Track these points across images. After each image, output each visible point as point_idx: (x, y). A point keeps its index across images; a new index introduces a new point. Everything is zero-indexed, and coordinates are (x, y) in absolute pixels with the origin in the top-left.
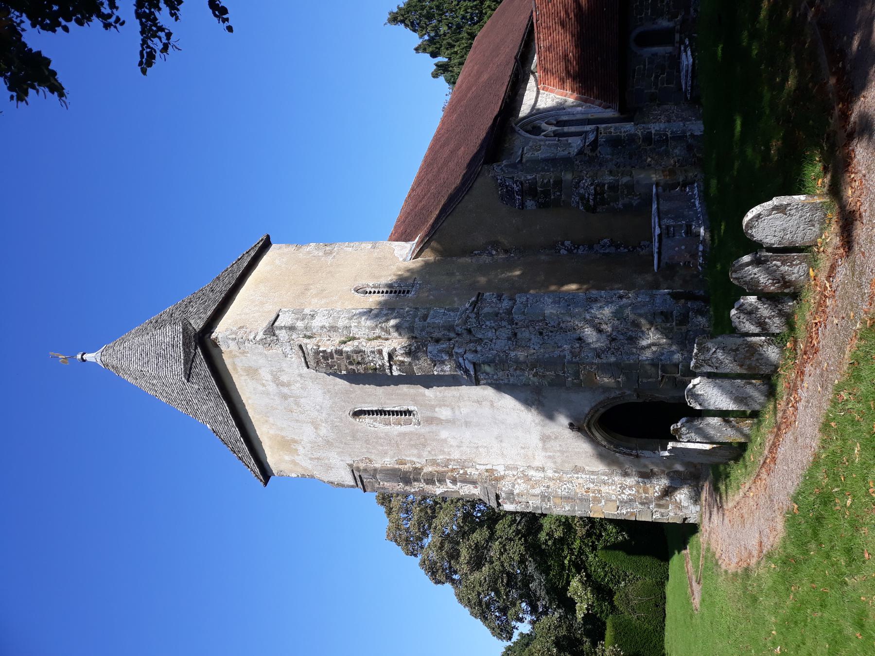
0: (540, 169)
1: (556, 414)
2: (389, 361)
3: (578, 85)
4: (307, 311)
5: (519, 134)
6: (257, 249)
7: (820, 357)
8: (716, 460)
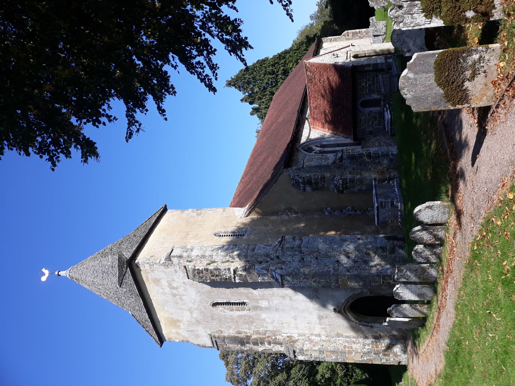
0: (313, 171)
2: (234, 274)
3: (331, 126)
4: (189, 247)
5: (301, 152)
6: (160, 212)
7: (453, 275)
8: (412, 327)
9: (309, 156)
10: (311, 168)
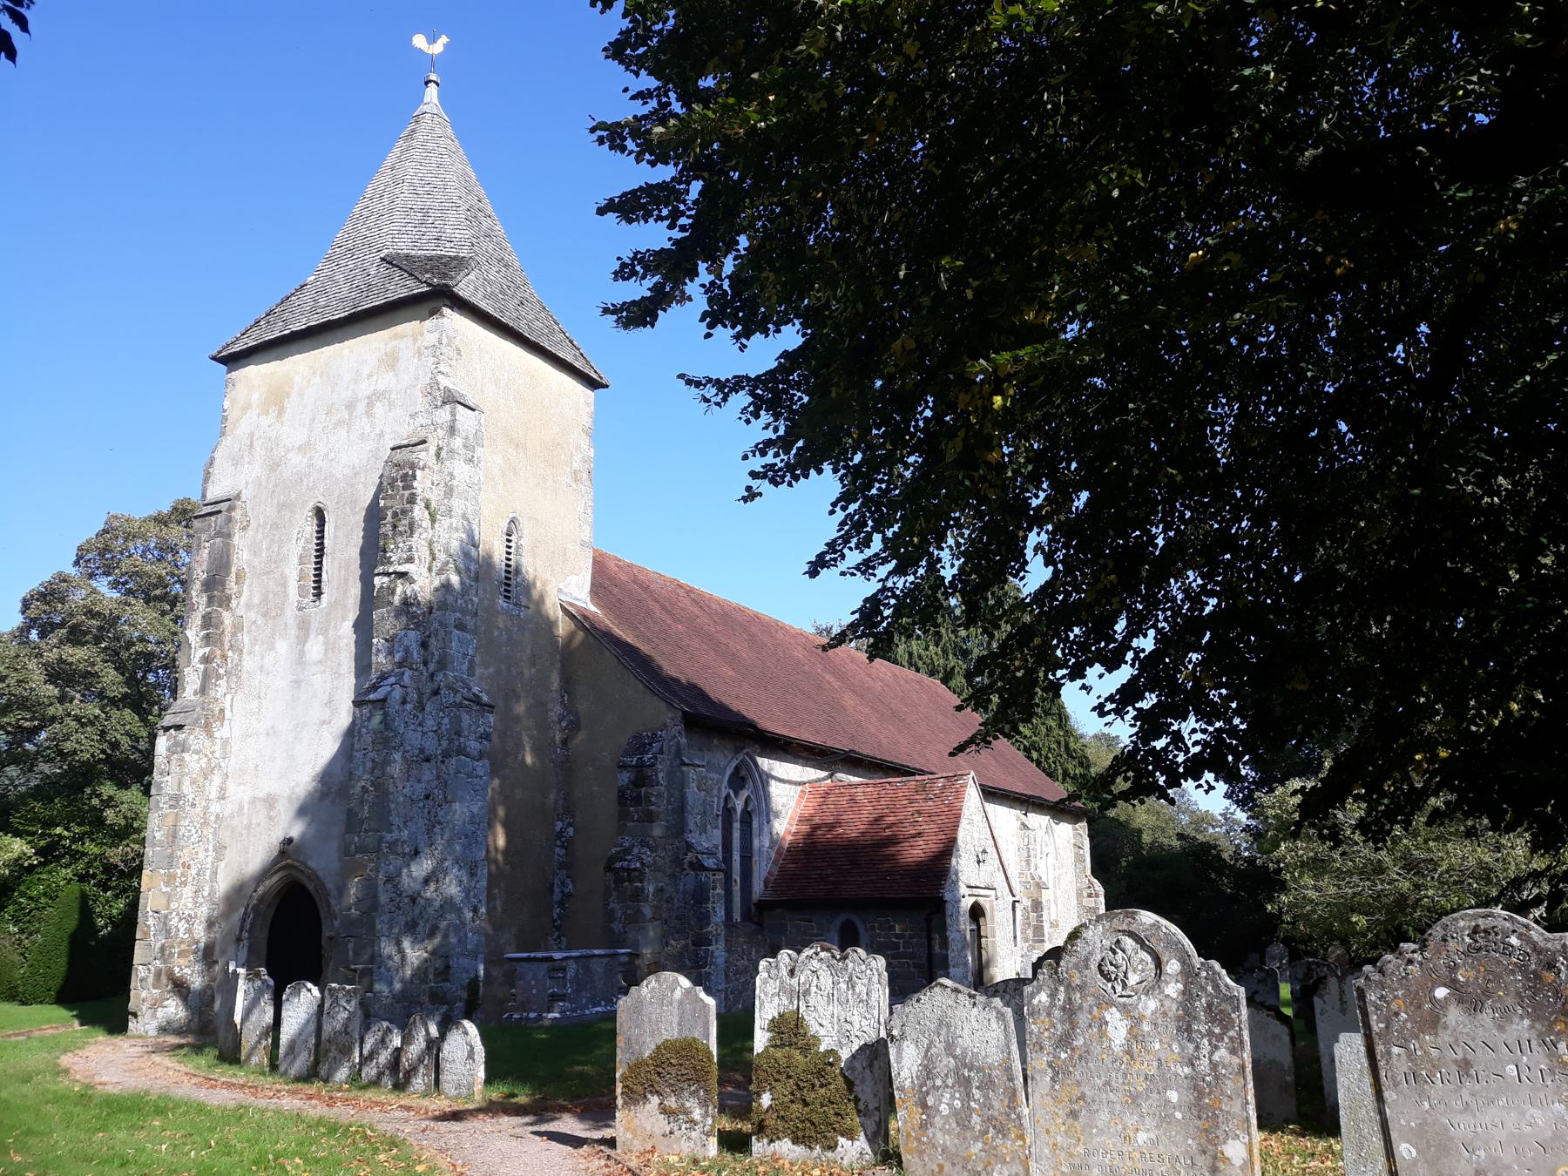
1: (308, 818)
2: (395, 573)
6: (587, 371)
8: (221, 1034)
9: (719, 782)
10: (679, 785)
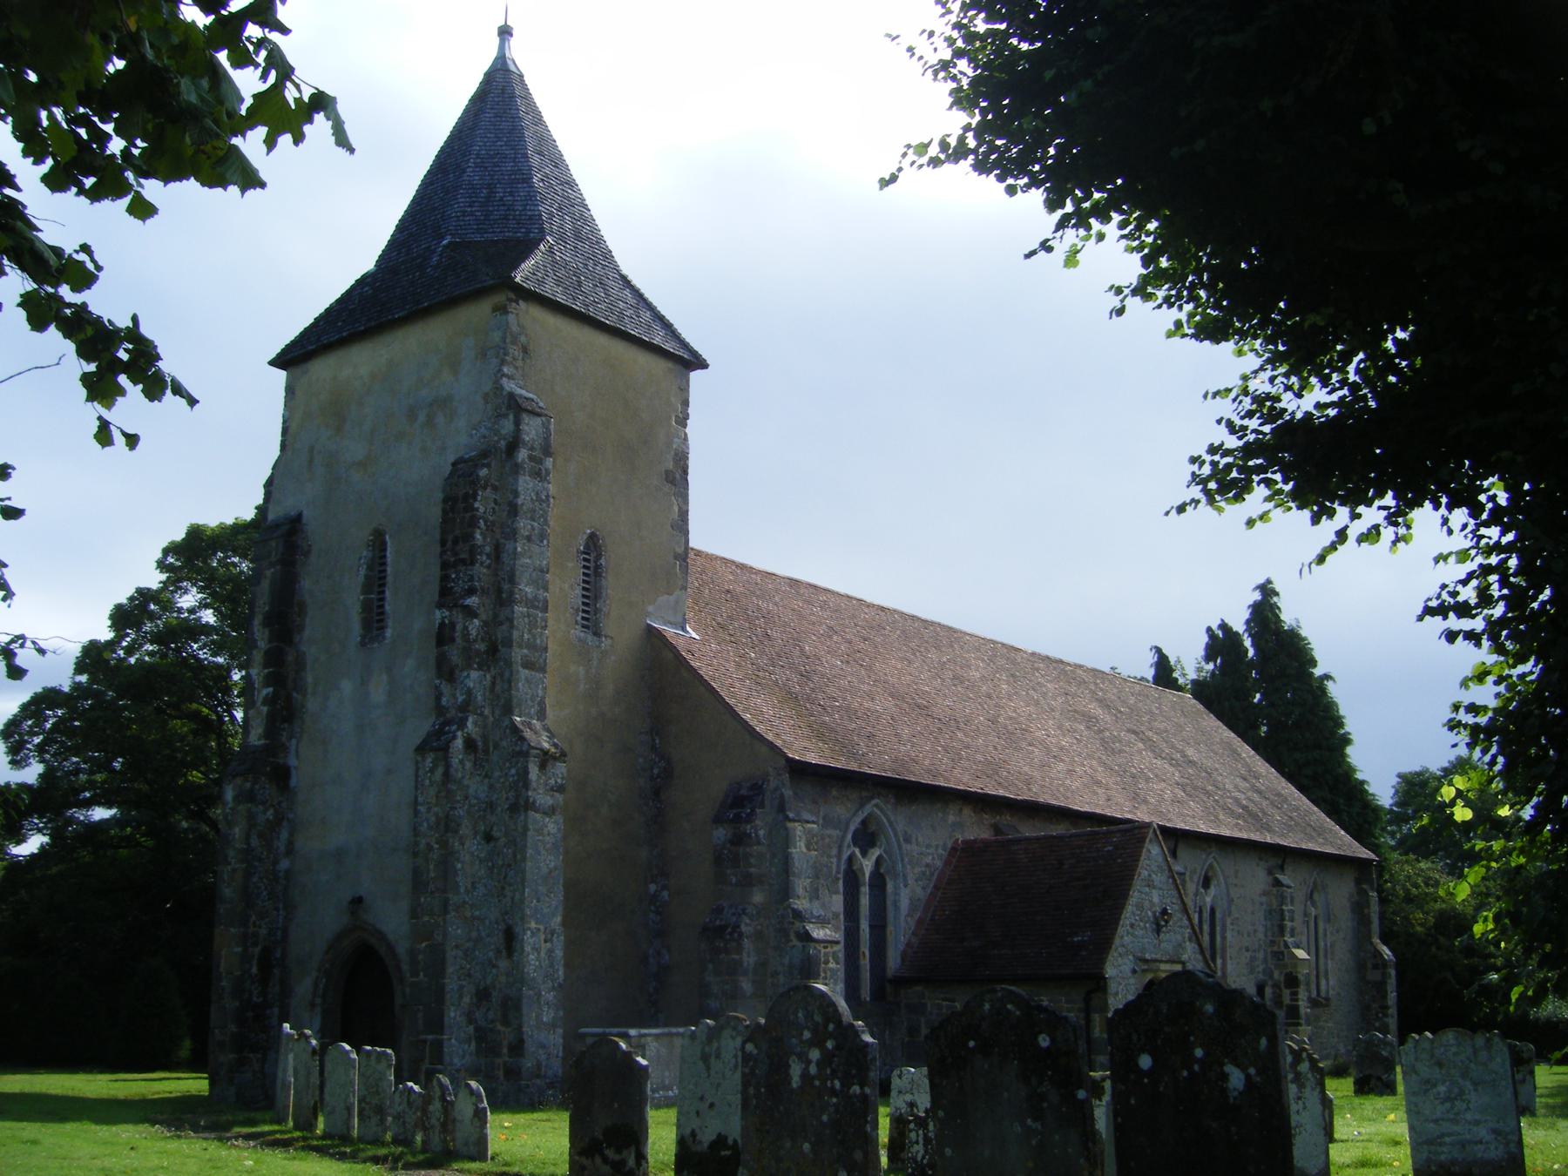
5: (857, 811)
